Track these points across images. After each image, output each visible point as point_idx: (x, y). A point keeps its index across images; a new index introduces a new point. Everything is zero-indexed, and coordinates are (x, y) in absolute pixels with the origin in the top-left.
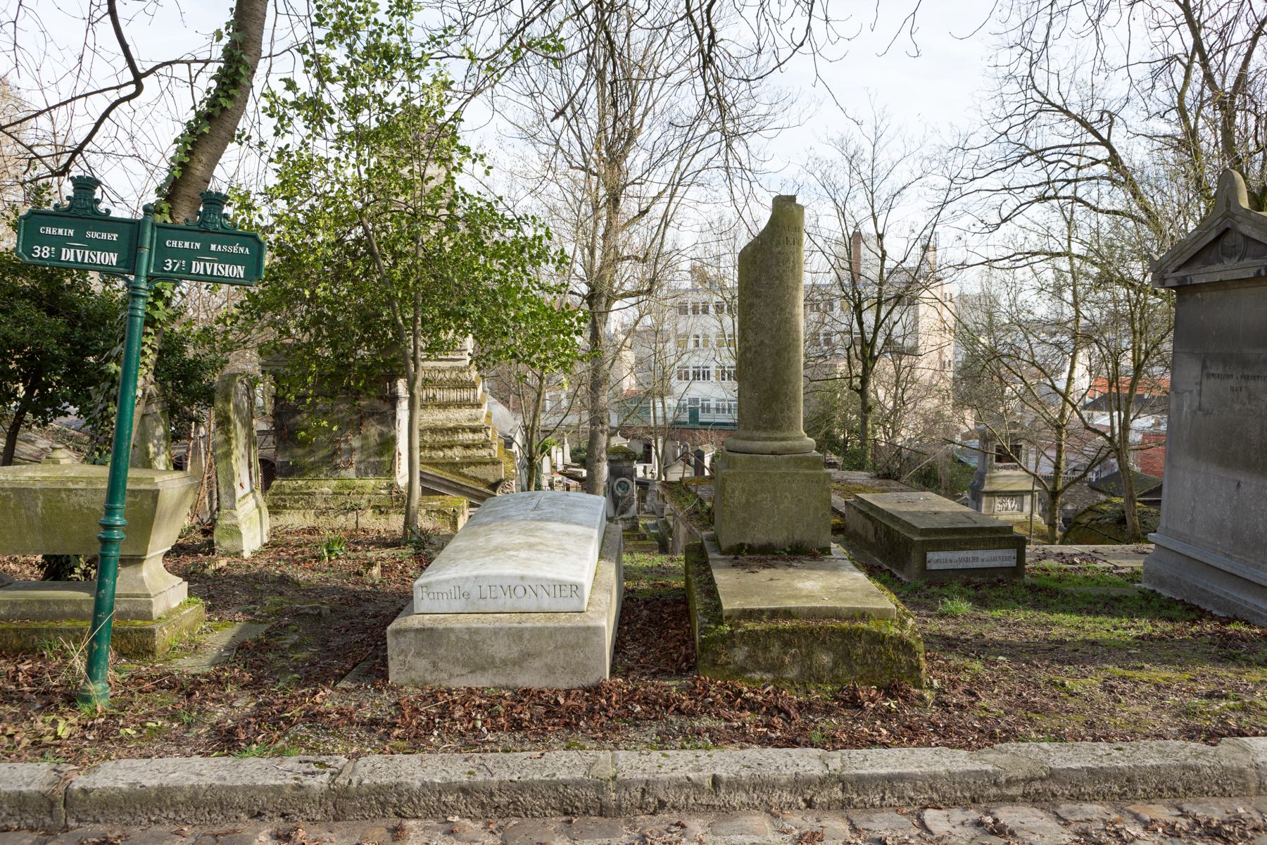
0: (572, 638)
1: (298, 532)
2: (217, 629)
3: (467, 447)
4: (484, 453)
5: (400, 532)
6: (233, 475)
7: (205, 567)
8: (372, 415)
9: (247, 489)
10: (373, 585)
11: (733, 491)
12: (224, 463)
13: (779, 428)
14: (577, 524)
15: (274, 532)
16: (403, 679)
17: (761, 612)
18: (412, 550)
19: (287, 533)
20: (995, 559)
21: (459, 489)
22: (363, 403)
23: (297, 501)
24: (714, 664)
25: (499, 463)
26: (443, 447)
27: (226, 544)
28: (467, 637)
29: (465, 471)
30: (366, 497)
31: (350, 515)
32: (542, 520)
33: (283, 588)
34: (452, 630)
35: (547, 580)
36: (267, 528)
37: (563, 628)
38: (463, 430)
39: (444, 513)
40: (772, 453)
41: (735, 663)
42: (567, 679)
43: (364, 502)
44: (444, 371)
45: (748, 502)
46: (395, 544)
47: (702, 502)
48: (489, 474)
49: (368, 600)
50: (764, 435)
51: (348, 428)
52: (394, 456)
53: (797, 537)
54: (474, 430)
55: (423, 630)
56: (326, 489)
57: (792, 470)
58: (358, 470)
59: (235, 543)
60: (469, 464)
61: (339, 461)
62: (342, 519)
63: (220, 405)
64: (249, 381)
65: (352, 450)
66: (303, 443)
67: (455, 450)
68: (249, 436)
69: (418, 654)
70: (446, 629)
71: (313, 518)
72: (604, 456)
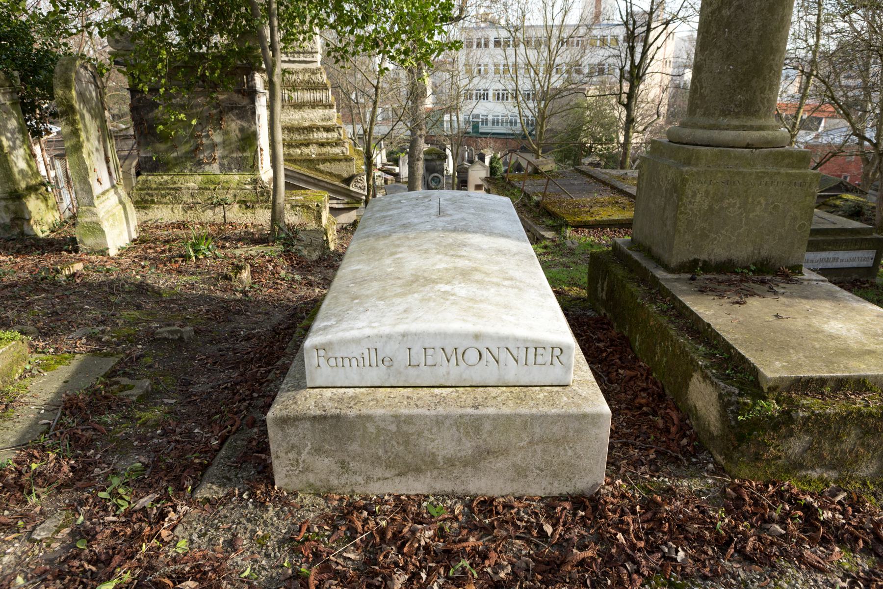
0: (557, 430)
1: (167, 227)
2: (47, 367)
3: (322, 145)
4: (337, 150)
5: (267, 231)
6: (86, 169)
7: (58, 271)
8: (231, 109)
9: (107, 184)
10: (244, 292)
11: (694, 195)
12: (75, 157)
13: (755, 114)
14: (503, 236)
15: (143, 227)
16: (296, 483)
17: (823, 381)
18: (281, 248)
19: (157, 227)
20: (854, 260)
21: (317, 184)
22: (221, 97)
23: (164, 196)
24: (757, 457)
25: (351, 160)
26: (299, 145)
27: (89, 242)
28: (393, 428)
29: (321, 167)
30: (232, 192)
31: (217, 209)
32: (455, 230)
33: (141, 300)
34: (369, 418)
35: (516, 339)
36: (134, 223)
37: (545, 416)
38: (318, 129)
39: (308, 208)
40: (748, 146)
41: (788, 457)
42: (544, 483)
43: (229, 197)
44: (297, 73)
45: (711, 208)
46: (262, 240)
47: (529, 197)
48: (343, 170)
49: (239, 313)
50: (736, 122)
51: (208, 123)
52: (256, 152)
53: (764, 253)
54: (328, 129)
55: (325, 418)
56: (191, 185)
57: (770, 169)
58: (222, 165)
59: (99, 241)
60: (324, 161)
61: (202, 156)
62: (209, 214)
63: (61, 92)
64: (93, 66)
65: (214, 146)
66: (163, 138)
67: (311, 147)
68: (103, 128)
69: (318, 451)
70: (359, 417)
71: (181, 213)
72: (422, 156)
